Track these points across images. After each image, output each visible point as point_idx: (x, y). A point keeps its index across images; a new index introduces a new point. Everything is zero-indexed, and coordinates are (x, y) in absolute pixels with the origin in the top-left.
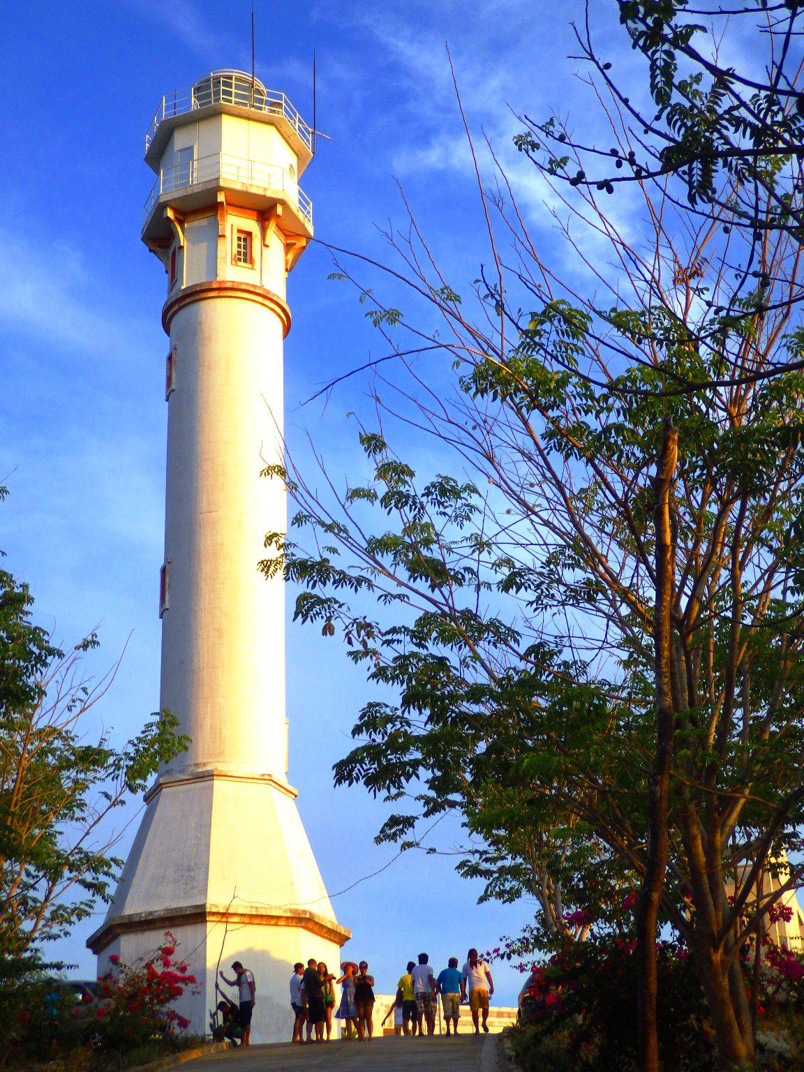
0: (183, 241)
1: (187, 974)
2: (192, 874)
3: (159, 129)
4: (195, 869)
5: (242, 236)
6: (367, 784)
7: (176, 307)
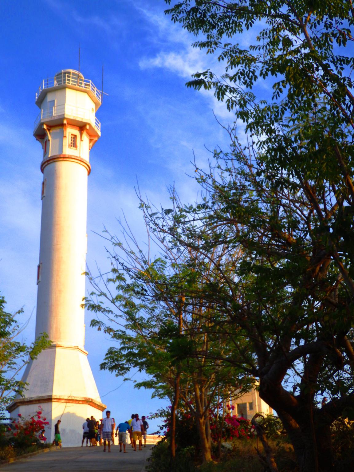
0: (50, 138)
1: (46, 421)
2: (47, 383)
3: (42, 92)
4: (49, 381)
5: (73, 136)
6: (109, 370)
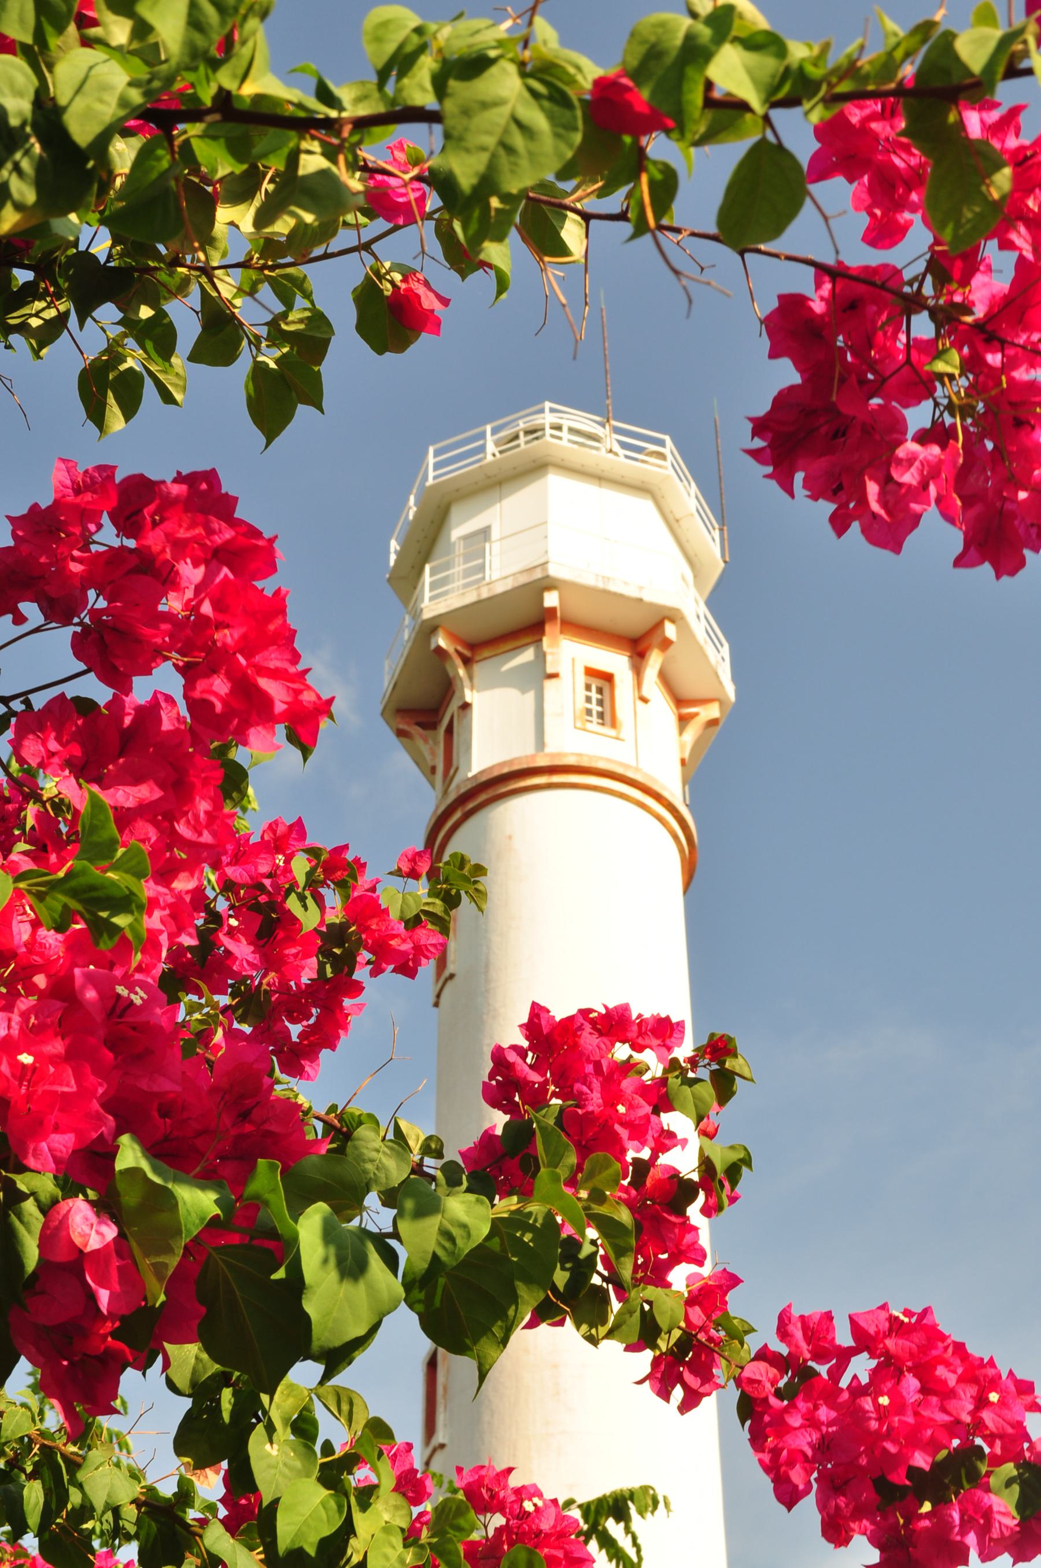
7: (458, 815)
